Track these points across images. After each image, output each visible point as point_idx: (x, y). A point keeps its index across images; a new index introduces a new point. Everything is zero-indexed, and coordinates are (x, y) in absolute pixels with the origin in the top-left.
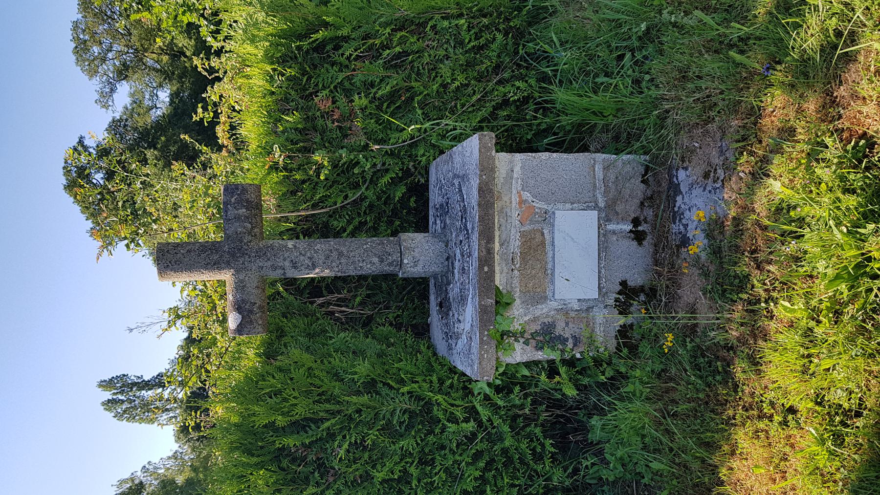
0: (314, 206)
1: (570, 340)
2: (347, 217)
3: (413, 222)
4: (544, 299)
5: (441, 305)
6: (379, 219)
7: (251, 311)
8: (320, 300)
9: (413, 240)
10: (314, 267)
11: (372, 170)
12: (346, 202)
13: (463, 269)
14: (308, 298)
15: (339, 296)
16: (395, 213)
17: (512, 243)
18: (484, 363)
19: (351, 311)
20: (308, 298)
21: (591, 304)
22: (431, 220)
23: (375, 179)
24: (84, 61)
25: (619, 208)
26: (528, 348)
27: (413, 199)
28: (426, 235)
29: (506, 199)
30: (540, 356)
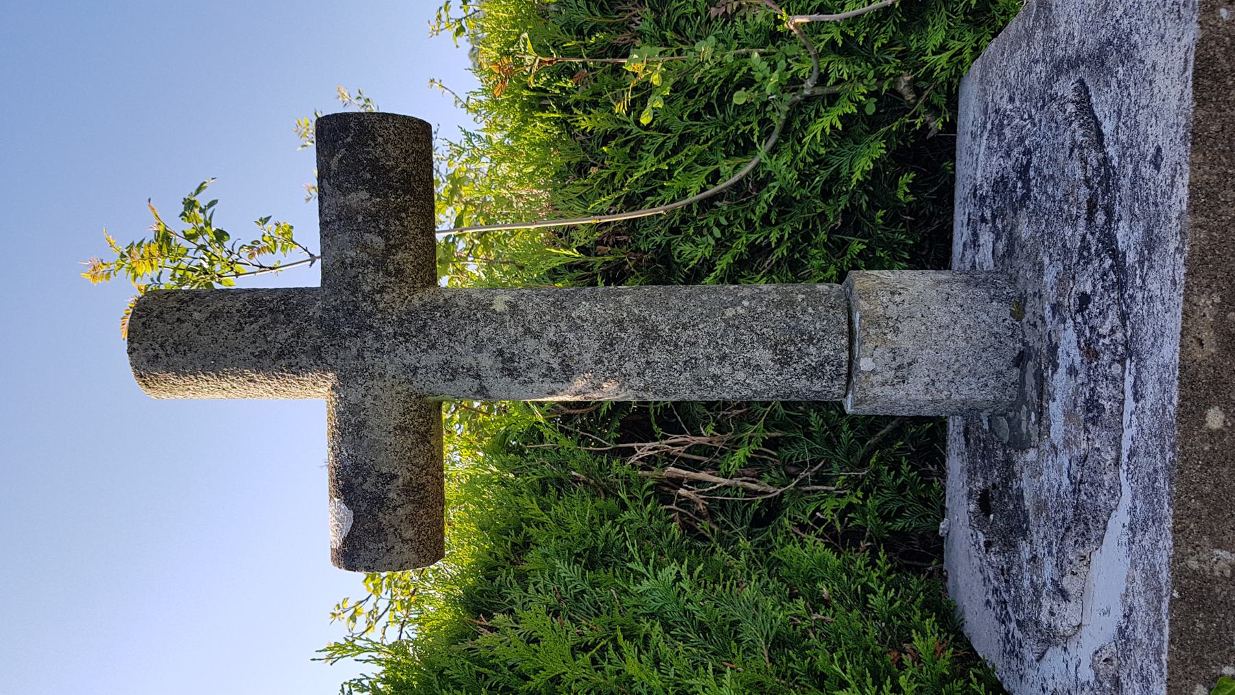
0: (631, 202)
2: (717, 232)
3: (904, 246)
5: (985, 503)
6: (807, 238)
7: (379, 501)
8: (644, 449)
9: (901, 297)
10: (567, 372)
11: (788, 97)
12: (712, 190)
13: (1092, 405)
14: (617, 441)
15: (697, 440)
16: (853, 221)
19: (726, 482)
20: (617, 441)
22: (961, 235)
23: (797, 124)
27: (906, 179)
28: (944, 275)
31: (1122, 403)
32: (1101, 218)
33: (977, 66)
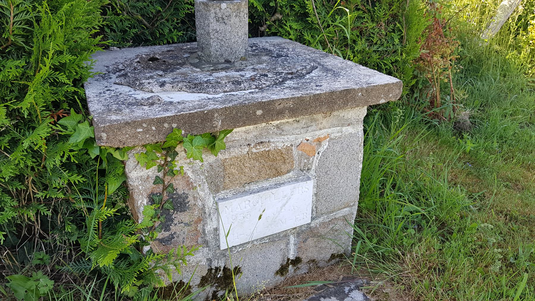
1: (167, 234)
4: (215, 188)
17: (281, 138)
18: (129, 131)
21: (212, 243)
26: (150, 185)
29: (324, 122)
31: (245, 90)
32: (290, 76)
33: (288, 41)
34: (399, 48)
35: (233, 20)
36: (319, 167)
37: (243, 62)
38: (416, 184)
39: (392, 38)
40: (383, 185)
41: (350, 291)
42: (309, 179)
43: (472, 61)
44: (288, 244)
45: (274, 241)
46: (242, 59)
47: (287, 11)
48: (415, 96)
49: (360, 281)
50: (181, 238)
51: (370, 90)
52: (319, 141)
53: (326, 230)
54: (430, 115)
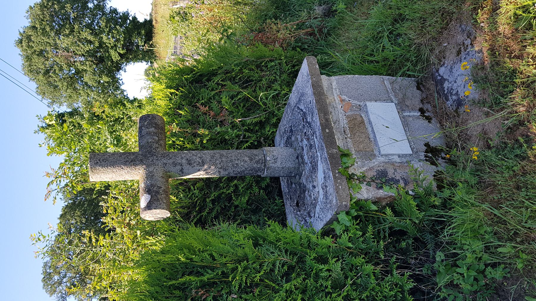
1: (401, 181)
7: (158, 192)
18: (341, 192)
21: (408, 159)
24: (48, 285)
25: (408, 103)
26: (371, 188)
30: (381, 193)
32: (305, 120)
33: (278, 132)
34: (277, 62)
35: (275, 154)
36: (358, 100)
37: (297, 149)
38: (369, 40)
39: (271, 67)
40: (372, 62)
41: (439, 75)
42: (366, 105)
43: (277, 7)
44: (409, 116)
45: (407, 124)
46: (295, 149)
47: (259, 134)
48: (306, 47)
49: (434, 70)
50: (404, 174)
51: (312, 74)
52: (342, 101)
53: (400, 94)
54: (320, 35)
